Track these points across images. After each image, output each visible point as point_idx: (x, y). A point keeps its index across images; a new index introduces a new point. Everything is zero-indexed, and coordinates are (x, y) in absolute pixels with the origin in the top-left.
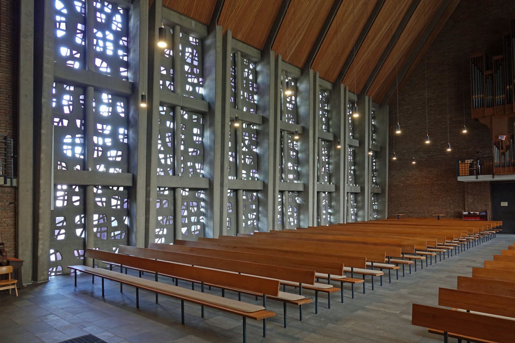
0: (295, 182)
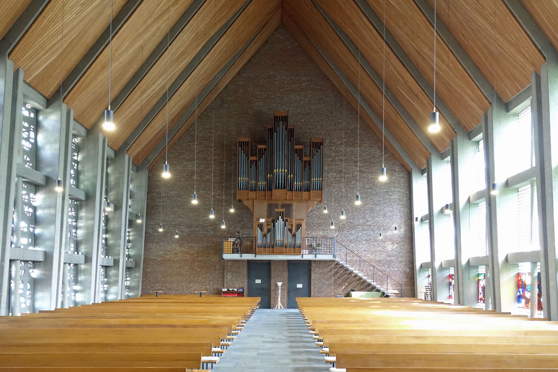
0: (31, 248)
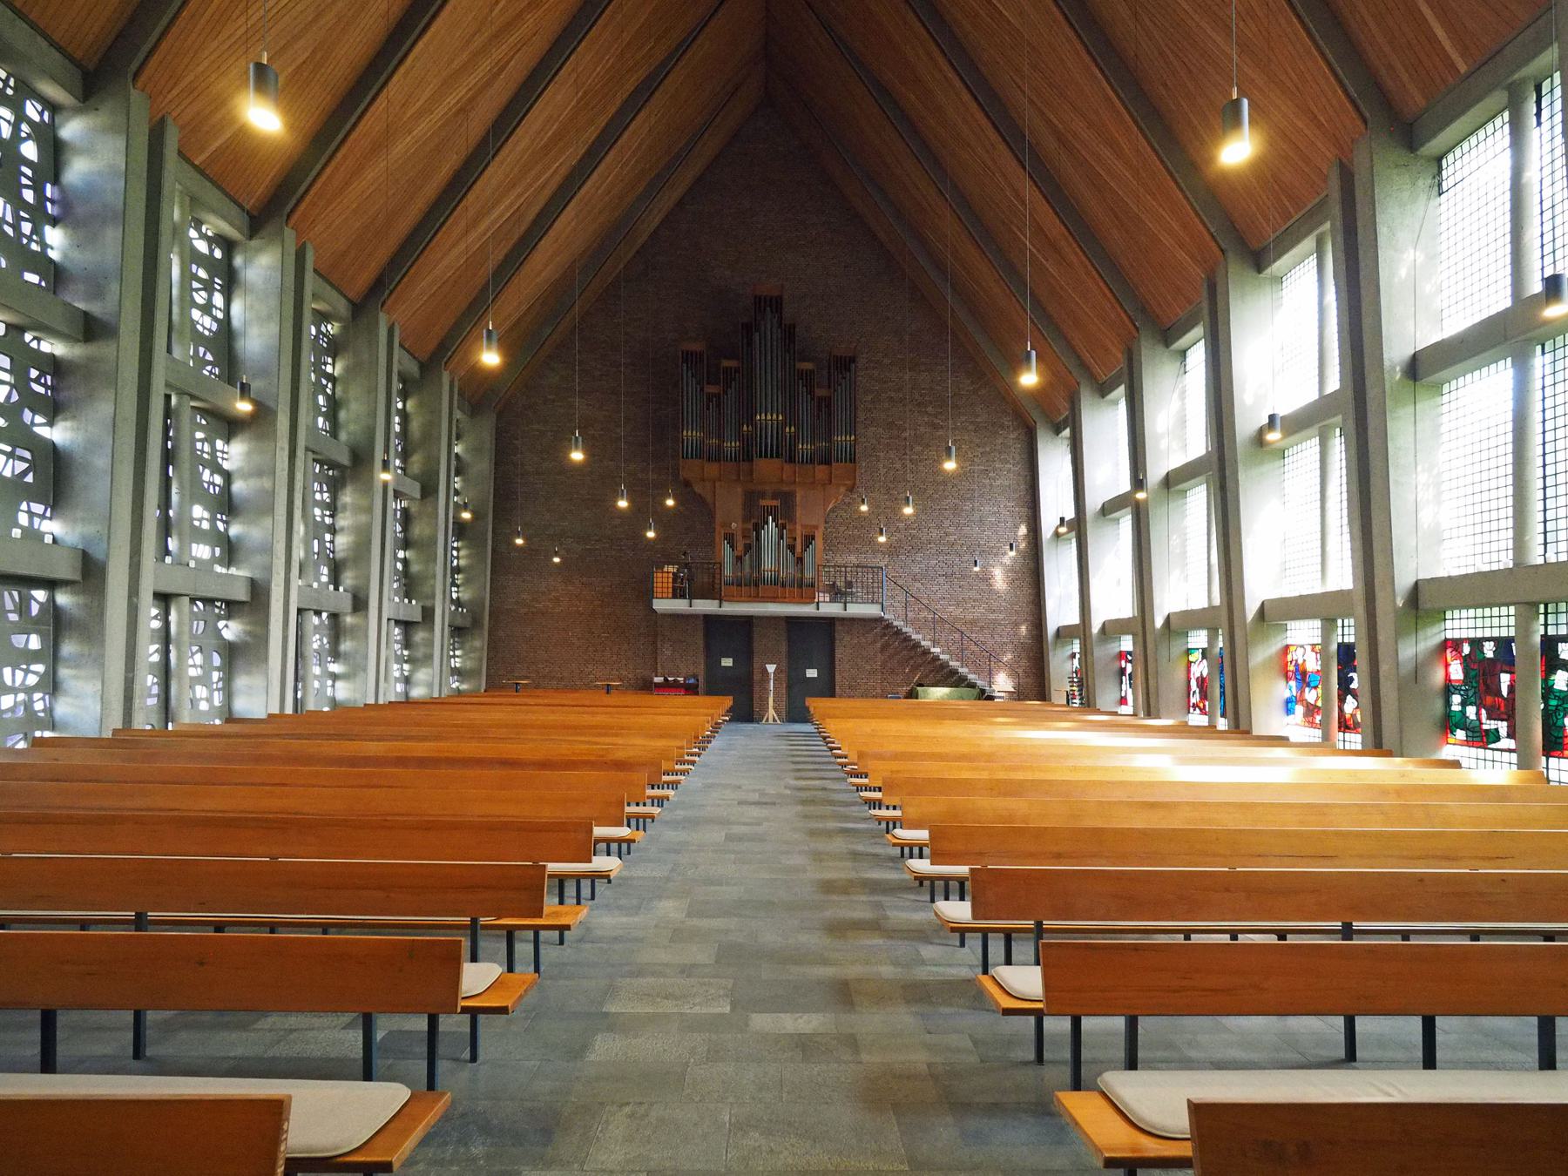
0: (219, 569)
